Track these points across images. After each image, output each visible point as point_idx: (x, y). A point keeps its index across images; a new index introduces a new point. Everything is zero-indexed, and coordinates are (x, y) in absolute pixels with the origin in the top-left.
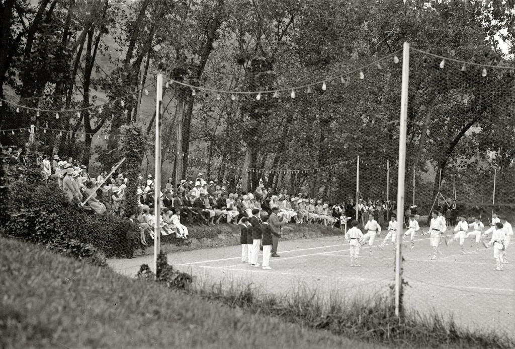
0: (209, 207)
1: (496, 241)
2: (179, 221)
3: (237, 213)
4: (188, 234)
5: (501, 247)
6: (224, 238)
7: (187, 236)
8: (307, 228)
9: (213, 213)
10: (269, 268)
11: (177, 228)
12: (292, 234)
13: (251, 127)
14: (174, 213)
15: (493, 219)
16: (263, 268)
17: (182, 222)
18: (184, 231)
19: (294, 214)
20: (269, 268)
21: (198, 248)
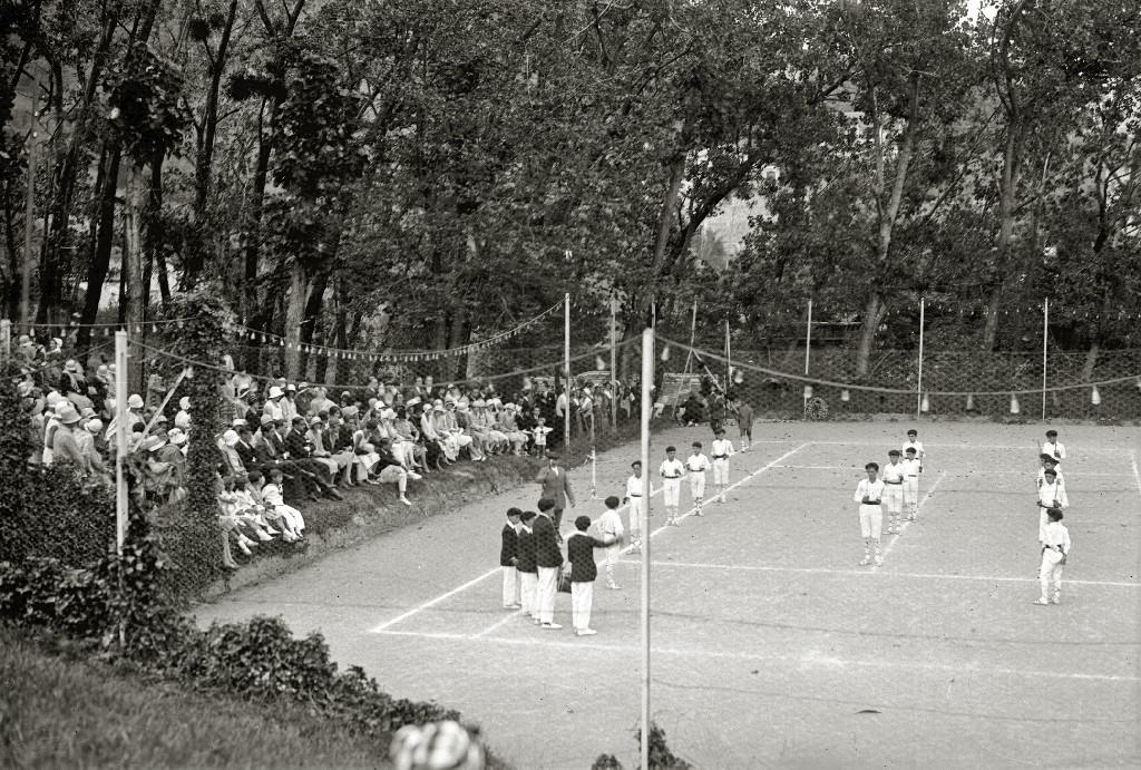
0: (324, 453)
1: (1048, 547)
2: (281, 497)
3: (376, 457)
4: (303, 527)
5: (1059, 556)
6: (362, 522)
7: (302, 531)
8: (496, 471)
9: (333, 464)
10: (589, 631)
11: (284, 518)
12: (473, 489)
13: (308, 222)
14: (269, 481)
15: (120, 268)
16: (580, 633)
17: (289, 498)
18: (295, 520)
19: (467, 439)
20: (589, 631)
21: (324, 553)
